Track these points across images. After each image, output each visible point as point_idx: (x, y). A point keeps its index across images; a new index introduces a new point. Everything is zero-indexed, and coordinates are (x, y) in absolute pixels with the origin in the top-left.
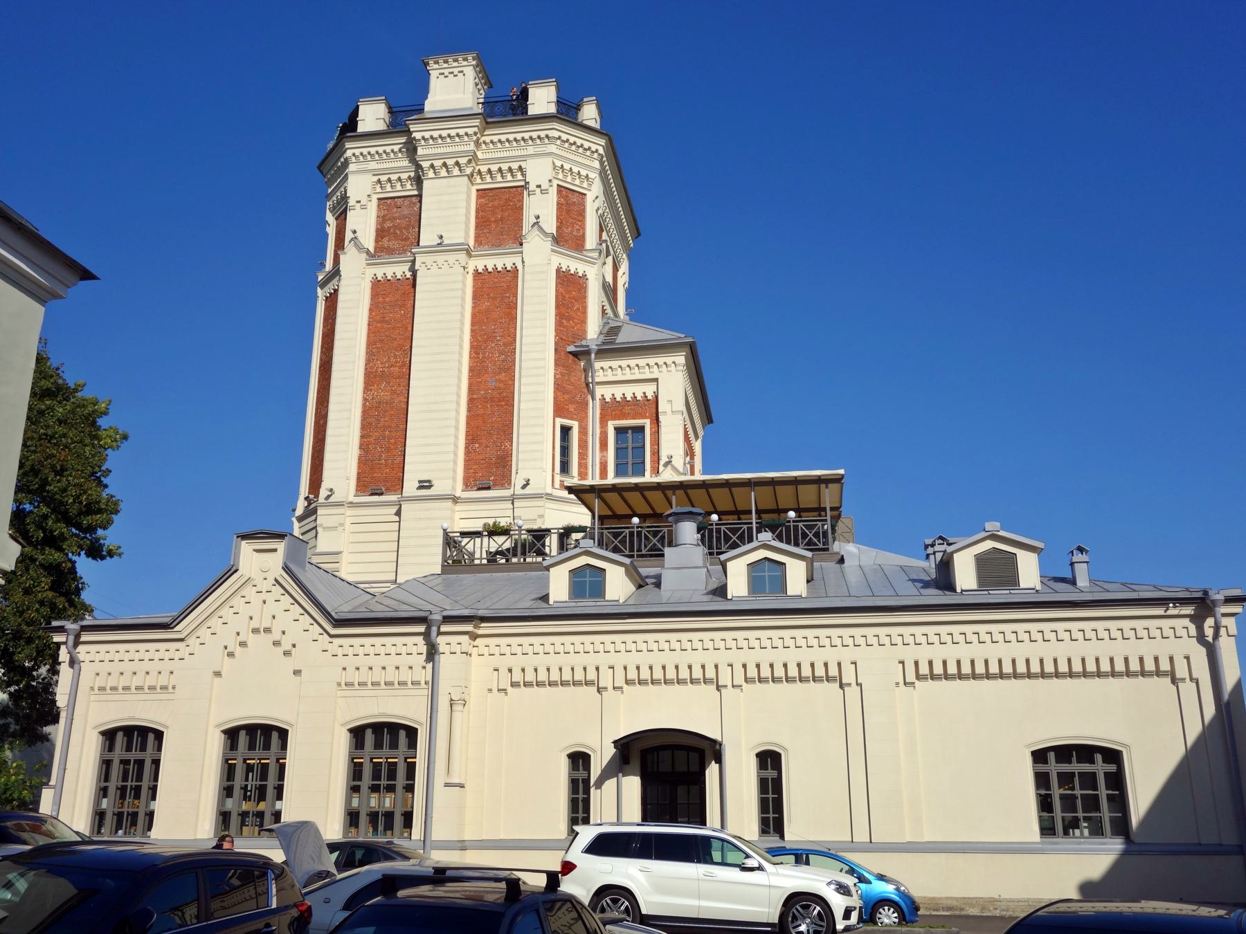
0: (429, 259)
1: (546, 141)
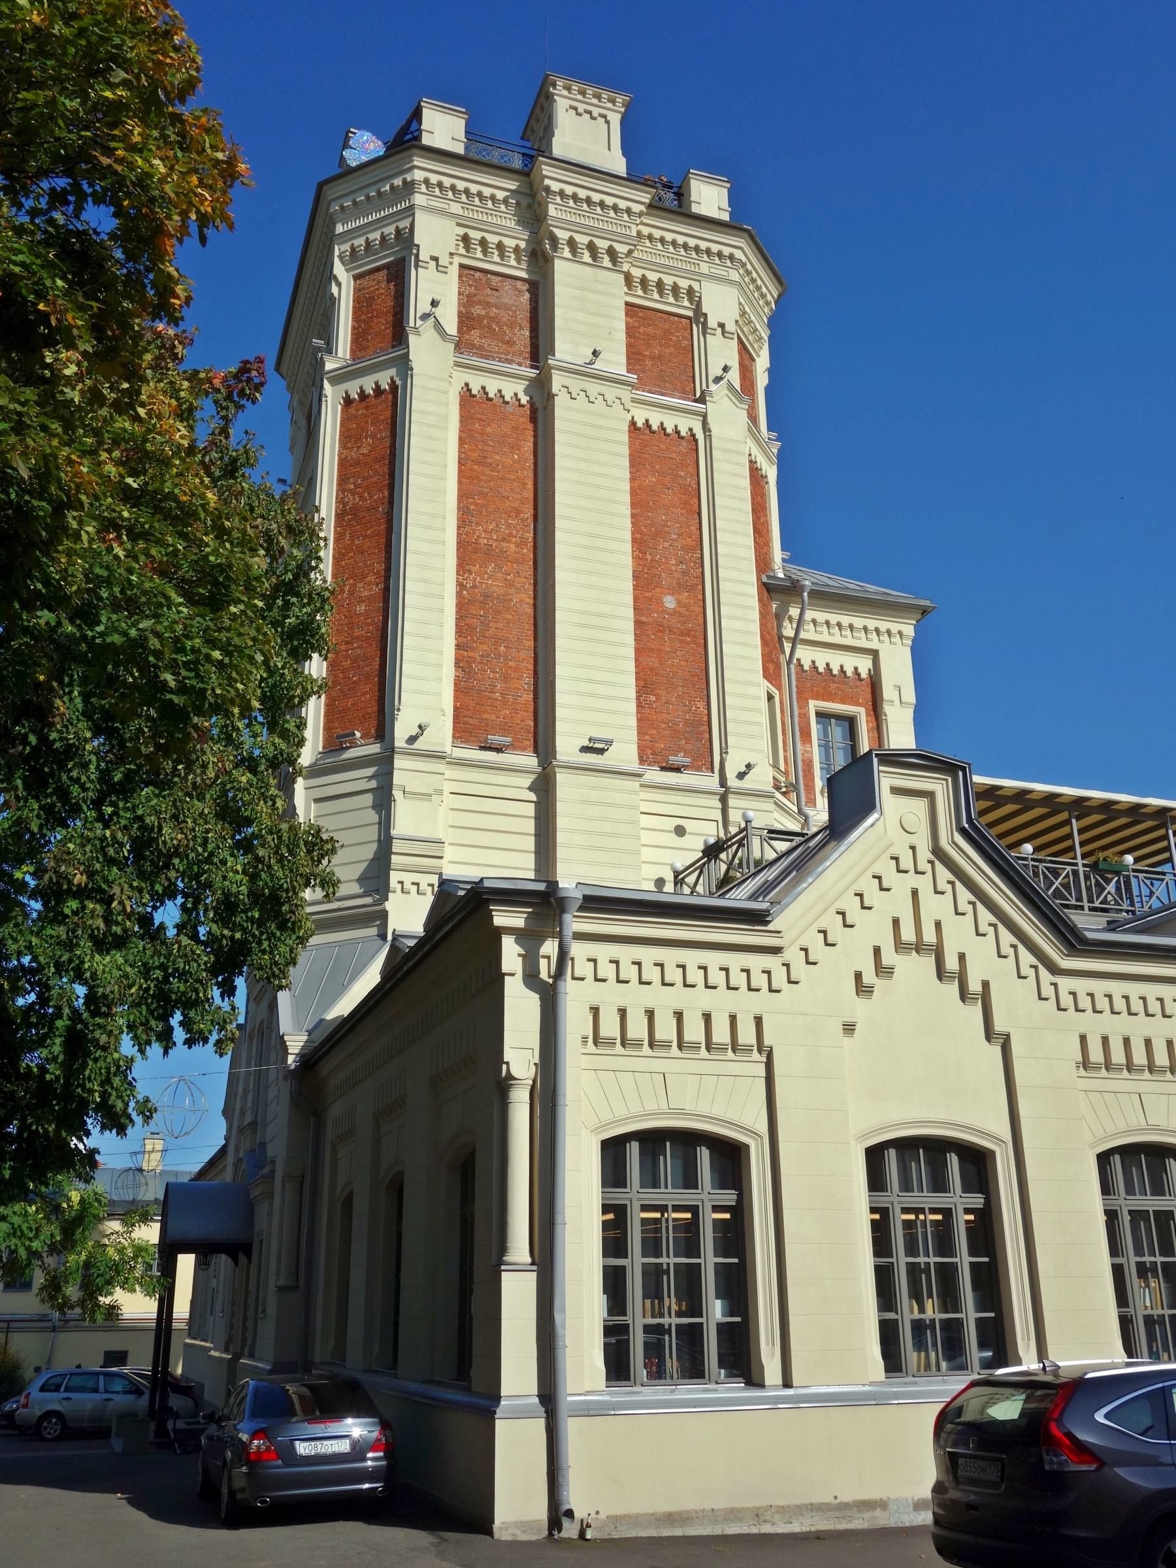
0: (575, 384)
1: (728, 263)
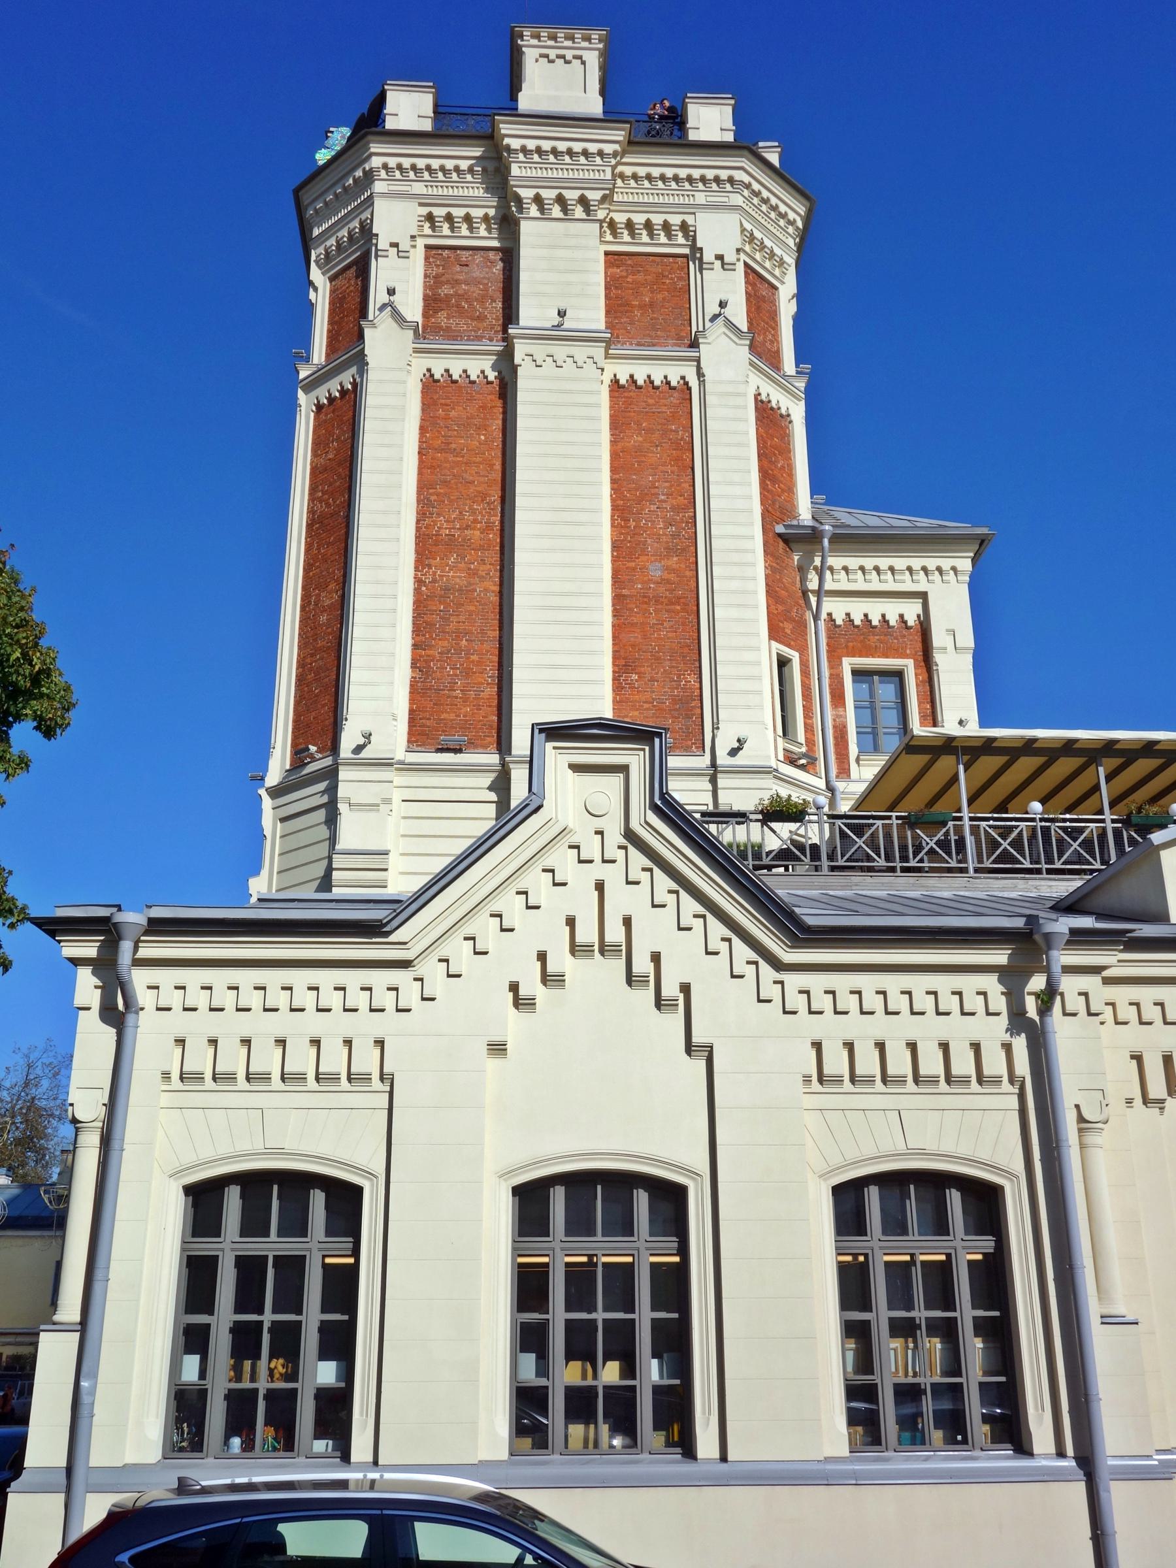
0: (540, 350)
1: (728, 187)
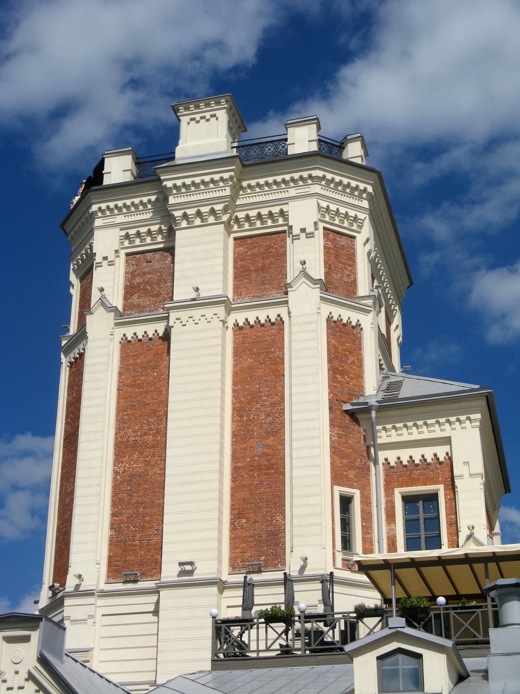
0: (184, 314)
